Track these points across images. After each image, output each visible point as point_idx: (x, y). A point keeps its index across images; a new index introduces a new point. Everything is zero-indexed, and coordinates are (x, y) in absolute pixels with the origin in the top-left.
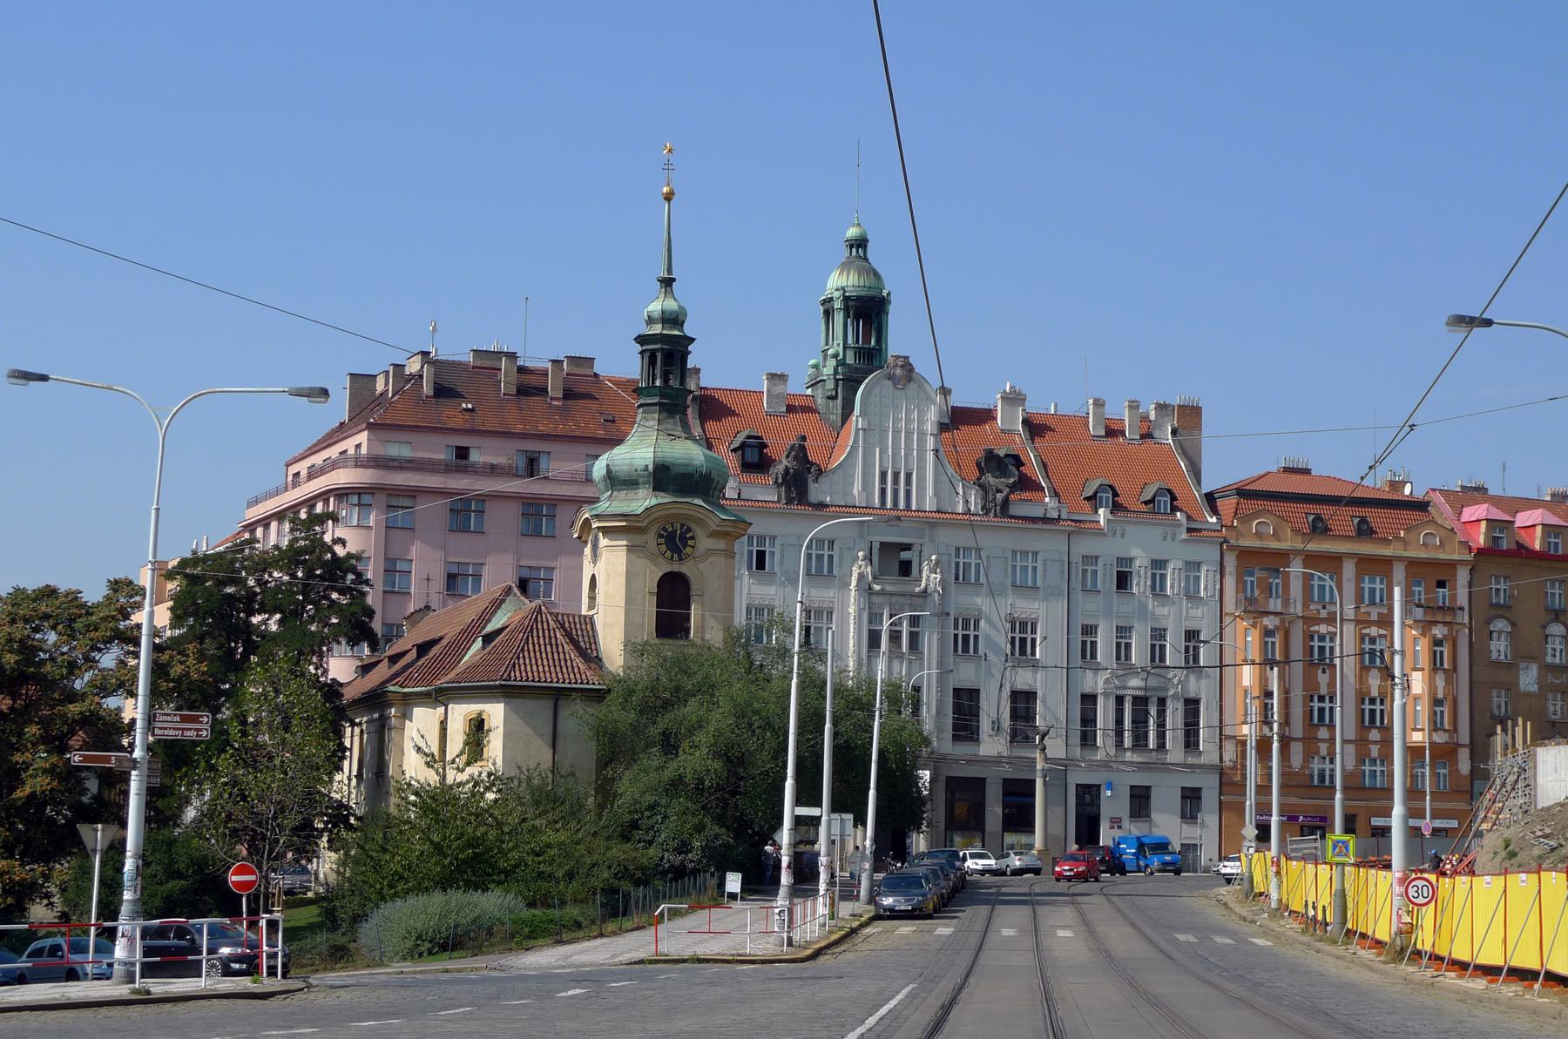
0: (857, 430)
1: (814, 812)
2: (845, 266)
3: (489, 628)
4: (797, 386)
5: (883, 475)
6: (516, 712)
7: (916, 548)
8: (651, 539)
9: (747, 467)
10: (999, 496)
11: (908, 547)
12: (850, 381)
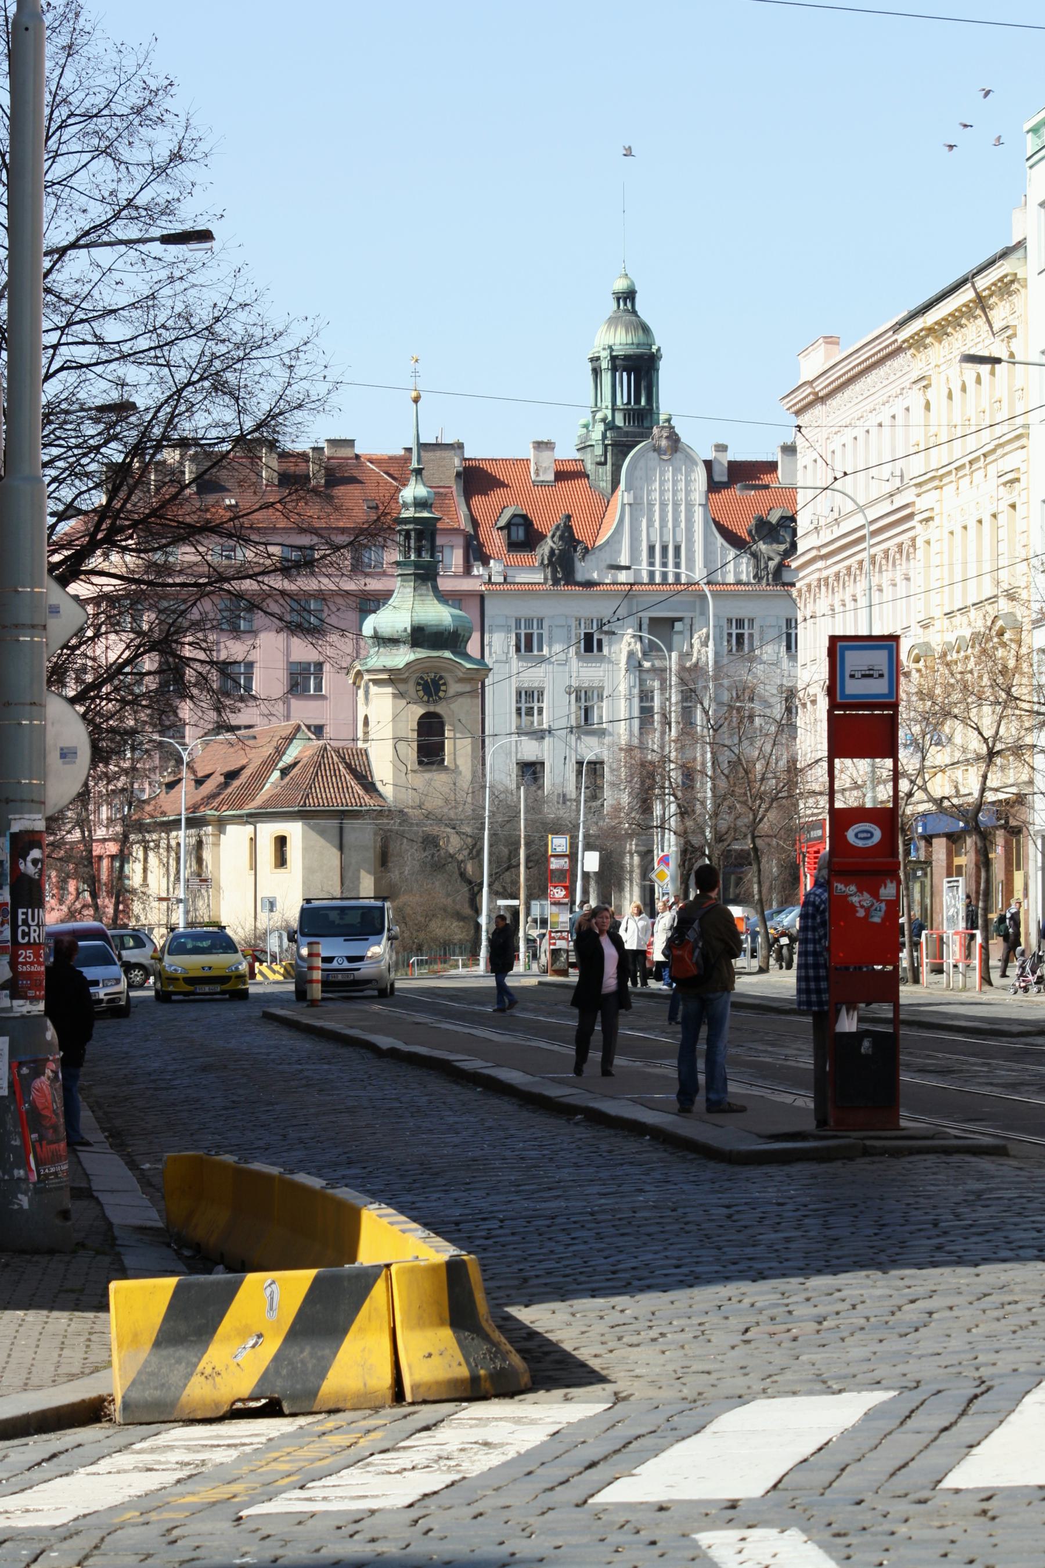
0: (623, 505)
1: (515, 902)
2: (613, 321)
3: (287, 759)
4: (566, 451)
5: (651, 549)
6: (312, 828)
7: (687, 621)
8: (411, 688)
9: (514, 546)
10: (772, 564)
11: (680, 619)
12: (620, 446)
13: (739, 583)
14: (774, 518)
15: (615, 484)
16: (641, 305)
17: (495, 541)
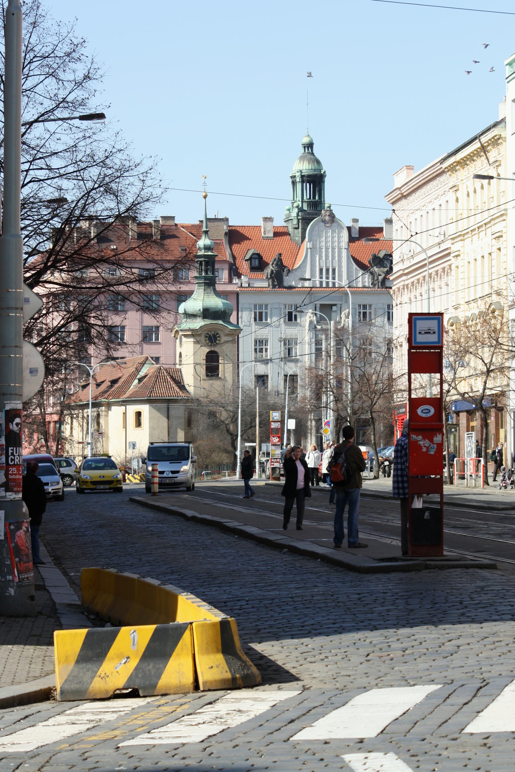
0: (307, 249)
1: (254, 444)
2: (302, 158)
3: (142, 374)
4: (279, 222)
5: (321, 270)
6: (154, 408)
7: (339, 306)
8: (202, 339)
9: (253, 269)
10: (380, 278)
11: (335, 305)
12: (305, 219)
13: (364, 287)
14: (381, 255)
15: (303, 238)
16: (316, 150)
17: (244, 266)
